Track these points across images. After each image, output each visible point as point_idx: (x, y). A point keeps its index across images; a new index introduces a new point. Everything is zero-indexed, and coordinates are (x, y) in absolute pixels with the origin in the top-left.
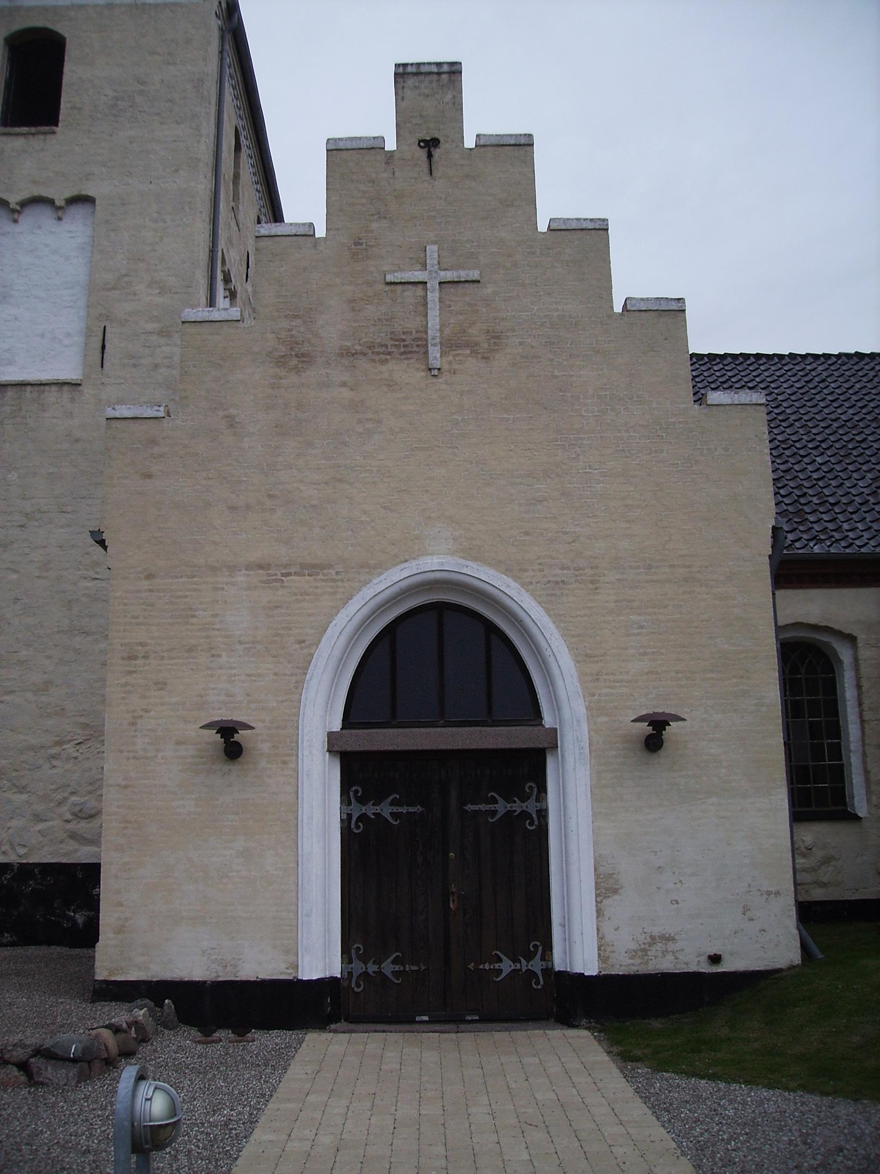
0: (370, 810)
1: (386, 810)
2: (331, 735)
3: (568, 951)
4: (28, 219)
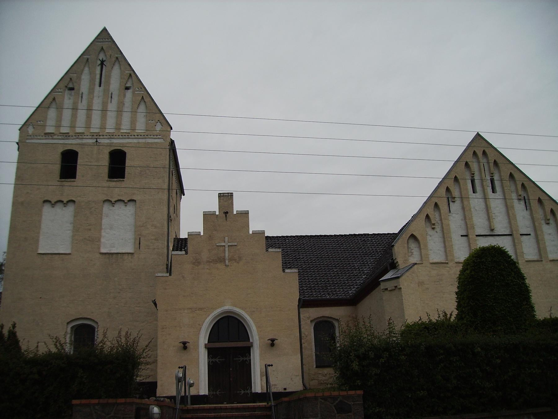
0: (214, 360)
1: (217, 360)
2: (205, 344)
3: (255, 388)
4: (117, 206)
